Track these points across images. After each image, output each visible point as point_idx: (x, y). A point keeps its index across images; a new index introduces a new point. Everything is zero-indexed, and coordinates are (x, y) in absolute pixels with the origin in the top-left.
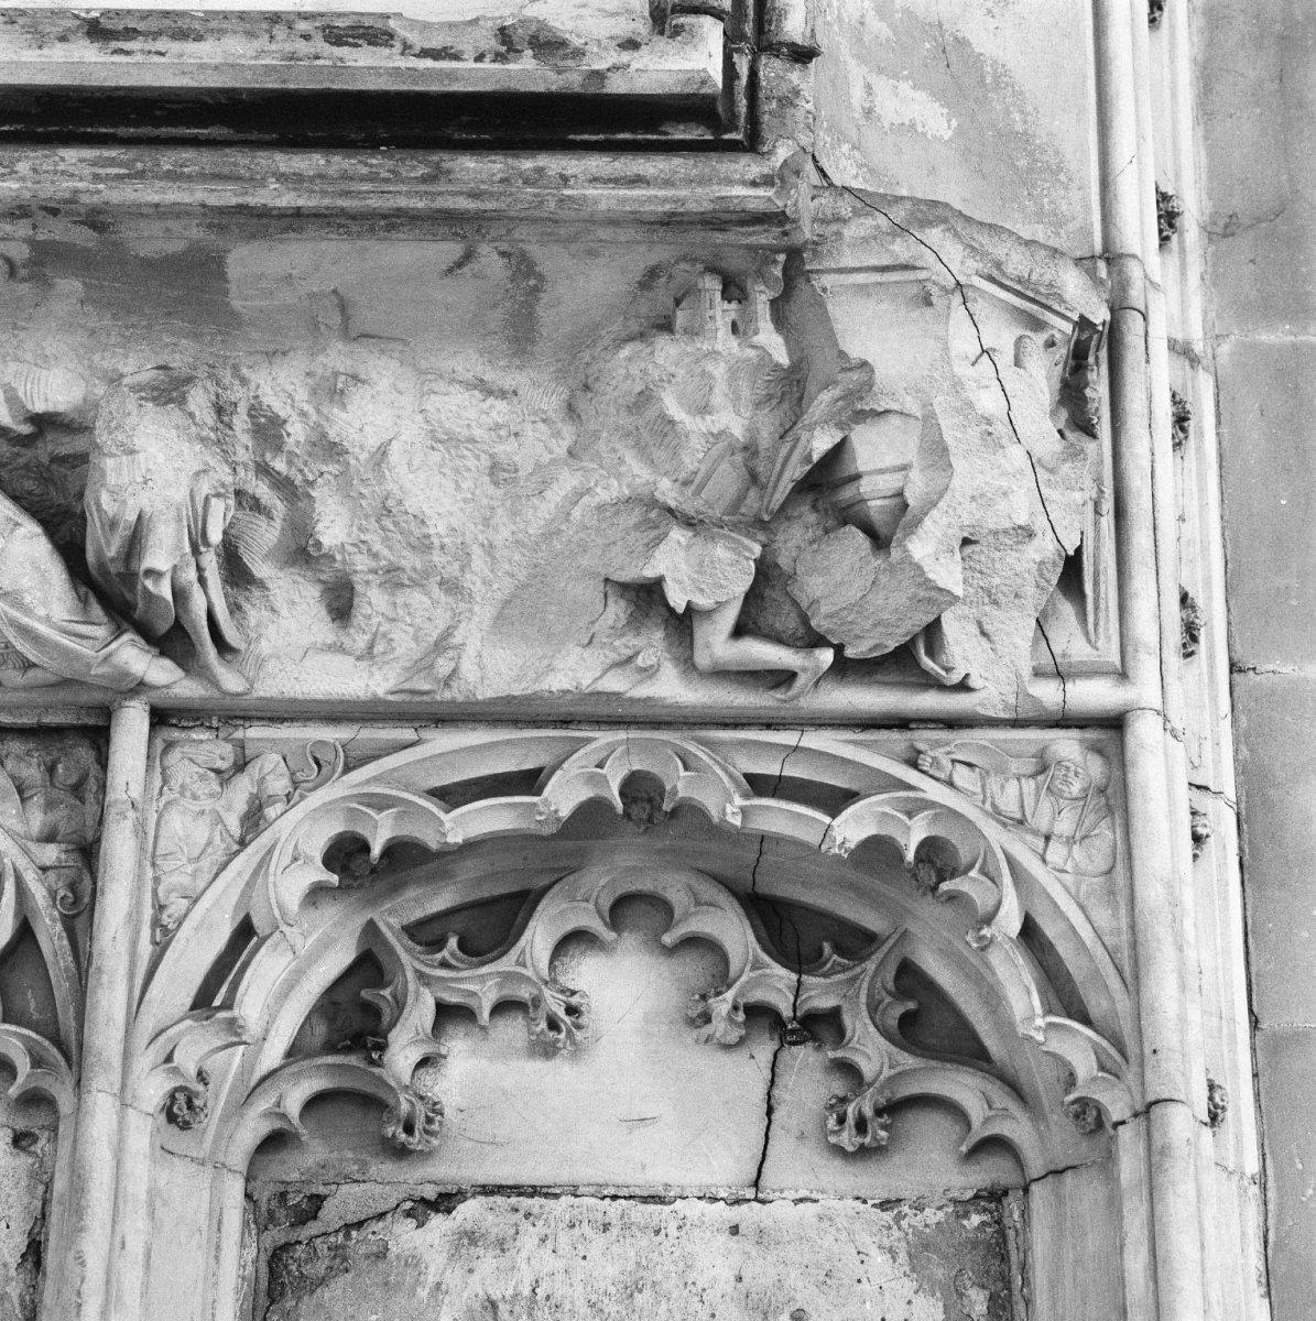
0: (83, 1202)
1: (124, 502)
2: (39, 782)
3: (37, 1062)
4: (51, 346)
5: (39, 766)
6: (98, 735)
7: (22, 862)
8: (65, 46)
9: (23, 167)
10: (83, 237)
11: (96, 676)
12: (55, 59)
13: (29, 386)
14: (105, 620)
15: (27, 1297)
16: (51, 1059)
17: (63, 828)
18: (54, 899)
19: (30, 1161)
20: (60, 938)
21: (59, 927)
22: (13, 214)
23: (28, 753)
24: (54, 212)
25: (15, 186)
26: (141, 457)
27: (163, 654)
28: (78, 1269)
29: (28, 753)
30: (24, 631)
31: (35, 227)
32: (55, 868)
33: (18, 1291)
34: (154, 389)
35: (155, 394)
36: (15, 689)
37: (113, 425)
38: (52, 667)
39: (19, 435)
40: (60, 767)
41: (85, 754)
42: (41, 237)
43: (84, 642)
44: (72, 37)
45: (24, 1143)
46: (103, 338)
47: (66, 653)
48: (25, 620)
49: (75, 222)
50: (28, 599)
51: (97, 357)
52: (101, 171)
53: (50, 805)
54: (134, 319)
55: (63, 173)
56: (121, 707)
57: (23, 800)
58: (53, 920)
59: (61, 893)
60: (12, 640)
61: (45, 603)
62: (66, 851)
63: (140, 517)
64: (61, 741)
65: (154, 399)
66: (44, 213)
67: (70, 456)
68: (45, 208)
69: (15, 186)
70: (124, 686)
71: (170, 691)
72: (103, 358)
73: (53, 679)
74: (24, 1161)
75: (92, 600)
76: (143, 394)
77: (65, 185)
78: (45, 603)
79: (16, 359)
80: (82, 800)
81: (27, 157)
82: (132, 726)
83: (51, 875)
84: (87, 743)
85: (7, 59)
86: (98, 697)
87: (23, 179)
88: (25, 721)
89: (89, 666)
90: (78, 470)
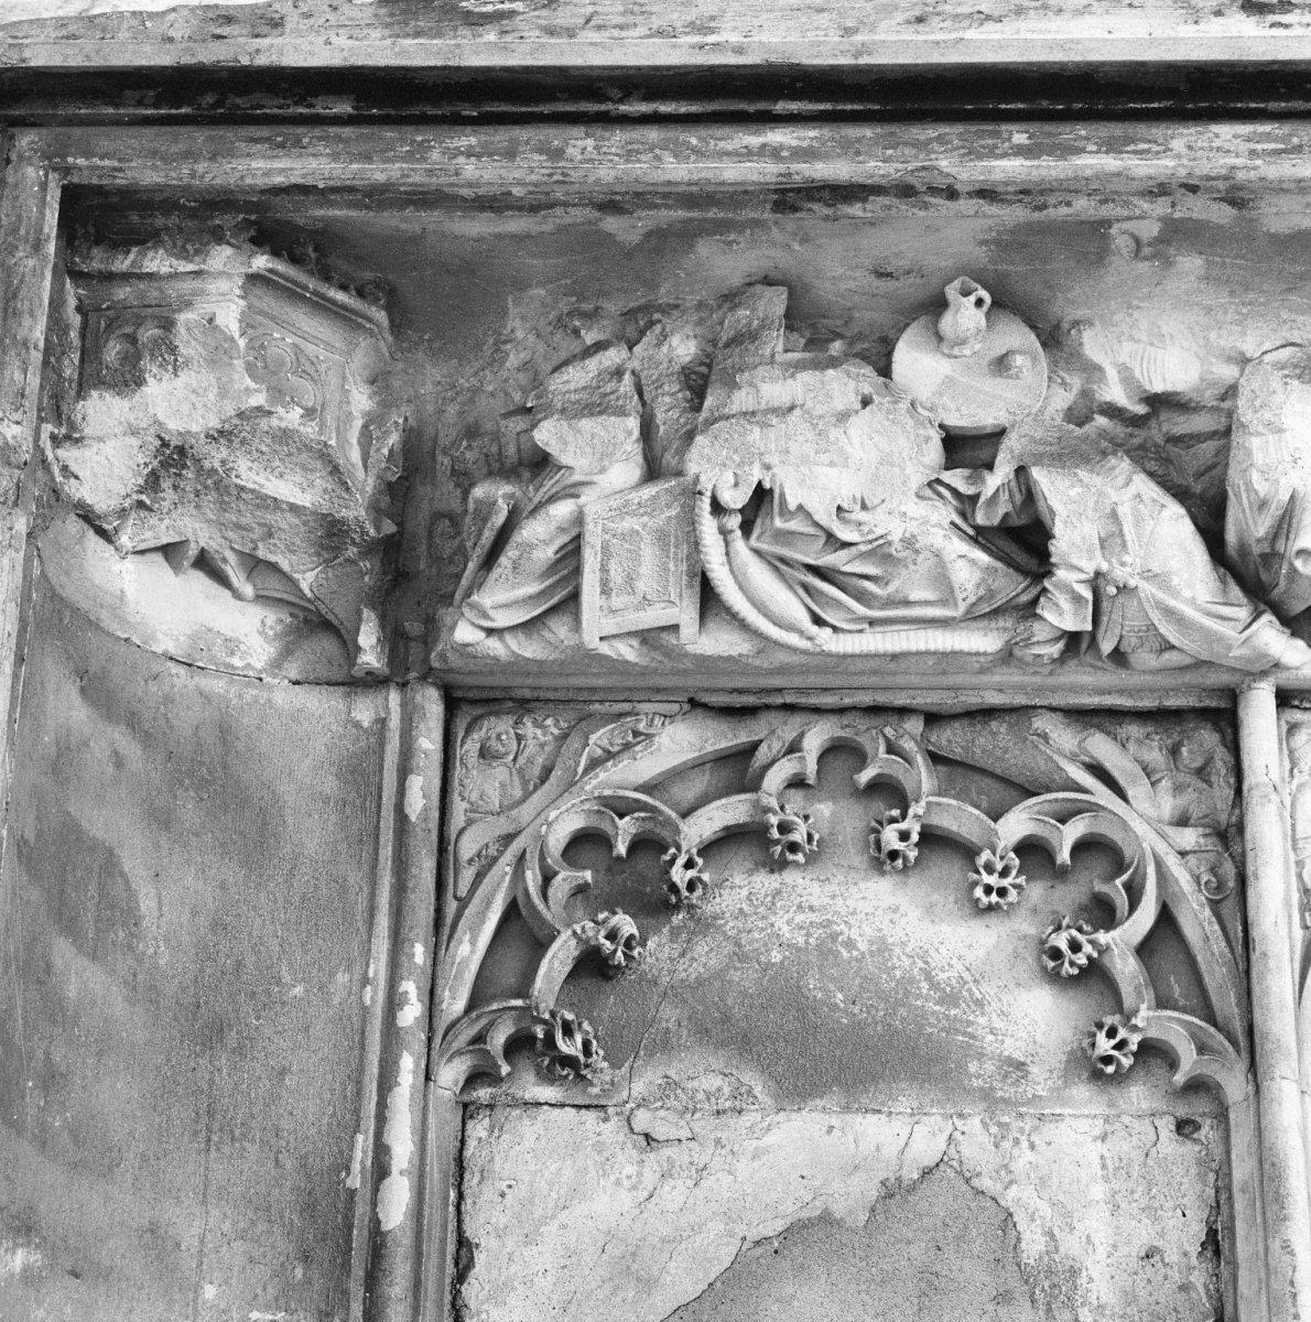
0: (1282, 1190)
1: (1277, 481)
2: (1163, 767)
3: (1202, 1049)
4: (1171, 324)
5: (1161, 749)
6: (1224, 716)
7: (1161, 848)
8: (1220, 20)
9: (1178, 145)
10: (1222, 214)
11: (1235, 658)
12: (1213, 34)
13: (1145, 365)
14: (1245, 601)
15: (1211, 1287)
16: (1216, 1046)
17: (1196, 813)
18: (1199, 884)
19: (1197, 1148)
20: (1210, 923)
21: (1207, 912)
22: (1151, 192)
23: (1147, 736)
24: (1193, 189)
25: (1171, 163)
26: (1287, 435)
27: (1294, 634)
28: (1287, 1258)
29: (1147, 736)
30: (1169, 613)
31: (1173, 205)
32: (1195, 852)
33: (1202, 1280)
34: (1296, 366)
35: (1297, 371)
36: (1144, 672)
37: (1257, 403)
38: (1193, 647)
39: (1136, 415)
40: (1184, 749)
41: (1208, 738)
42: (1177, 215)
43: (1226, 623)
44: (1227, 11)
45: (1186, 1131)
46: (1220, 316)
47: (1209, 636)
48: (1172, 603)
49: (1215, 199)
50: (1175, 581)
51: (1213, 335)
52: (1259, 147)
53: (1178, 789)
54: (1251, 296)
55: (1218, 149)
56: (1250, 688)
57: (1153, 784)
58: (1202, 906)
59: (1205, 878)
60: (1156, 622)
61: (1190, 586)
62: (1205, 836)
63: (1292, 496)
64: (1180, 724)
65: (1299, 377)
66: (1183, 190)
67: (1185, 436)
68: (1184, 186)
69: (1171, 163)
70: (1257, 667)
71: (1300, 673)
72: (1219, 337)
73: (1188, 661)
74: (1190, 1149)
75: (1229, 576)
76: (1286, 372)
77: (1222, 161)
78: (1190, 586)
79: (1131, 338)
80: (1209, 783)
81: (1182, 134)
82: (1260, 714)
83: (1192, 859)
84: (1209, 726)
85: (1165, 36)
86: (1224, 679)
87: (1179, 156)
88: (1147, 704)
89: (1229, 648)
90: (1192, 451)
